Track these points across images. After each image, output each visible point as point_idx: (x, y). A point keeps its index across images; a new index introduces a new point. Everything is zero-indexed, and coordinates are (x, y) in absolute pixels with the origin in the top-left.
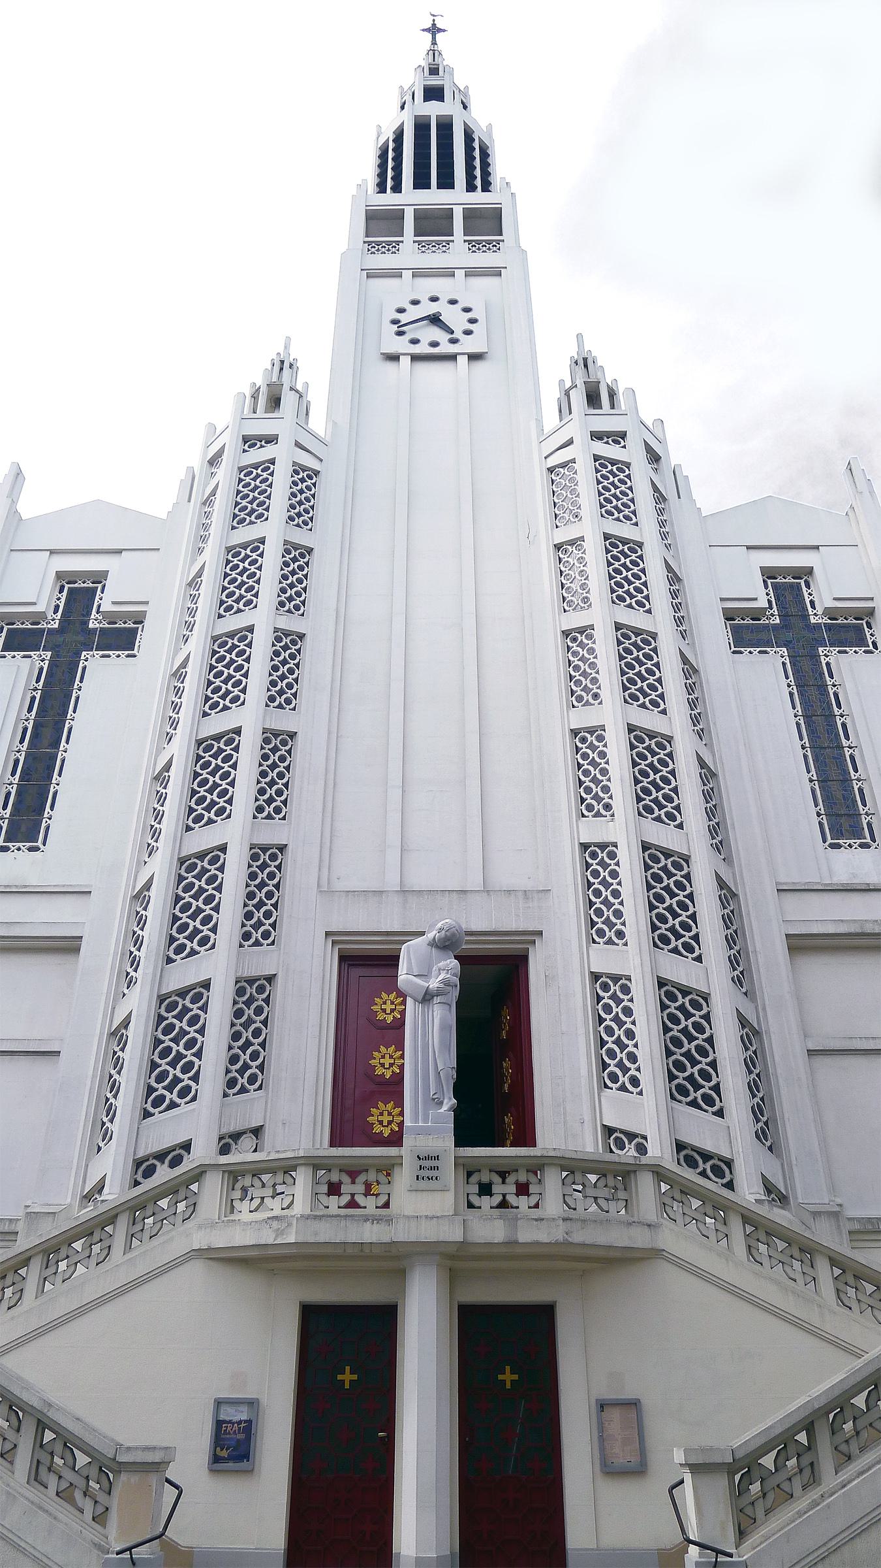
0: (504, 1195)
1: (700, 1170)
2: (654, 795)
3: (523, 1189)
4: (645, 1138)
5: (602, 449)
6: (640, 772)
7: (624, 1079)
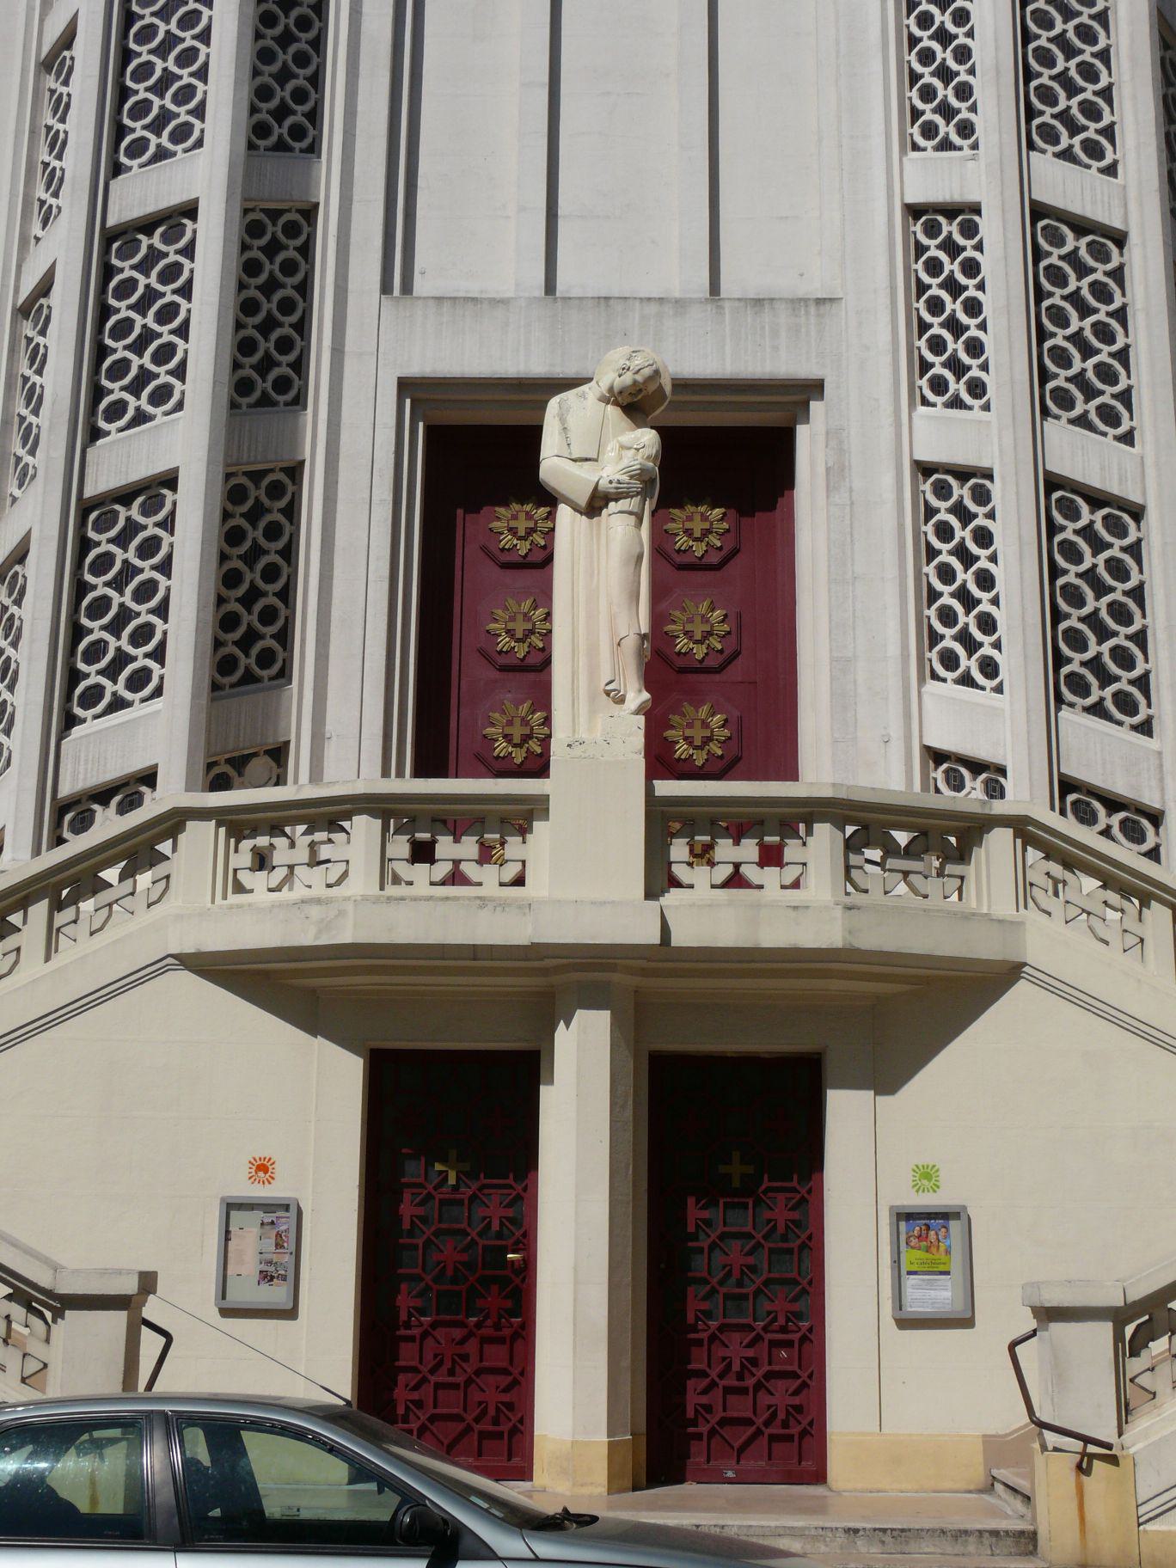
0: (737, 866)
1: (1101, 826)
2: (1061, 64)
3: (771, 857)
4: (1002, 771)
7: (957, 387)
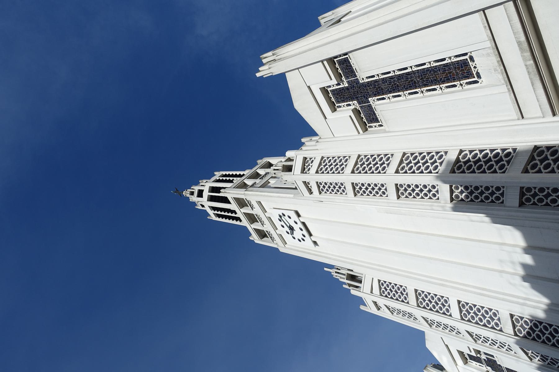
5: (313, 170)
6: (478, 169)
